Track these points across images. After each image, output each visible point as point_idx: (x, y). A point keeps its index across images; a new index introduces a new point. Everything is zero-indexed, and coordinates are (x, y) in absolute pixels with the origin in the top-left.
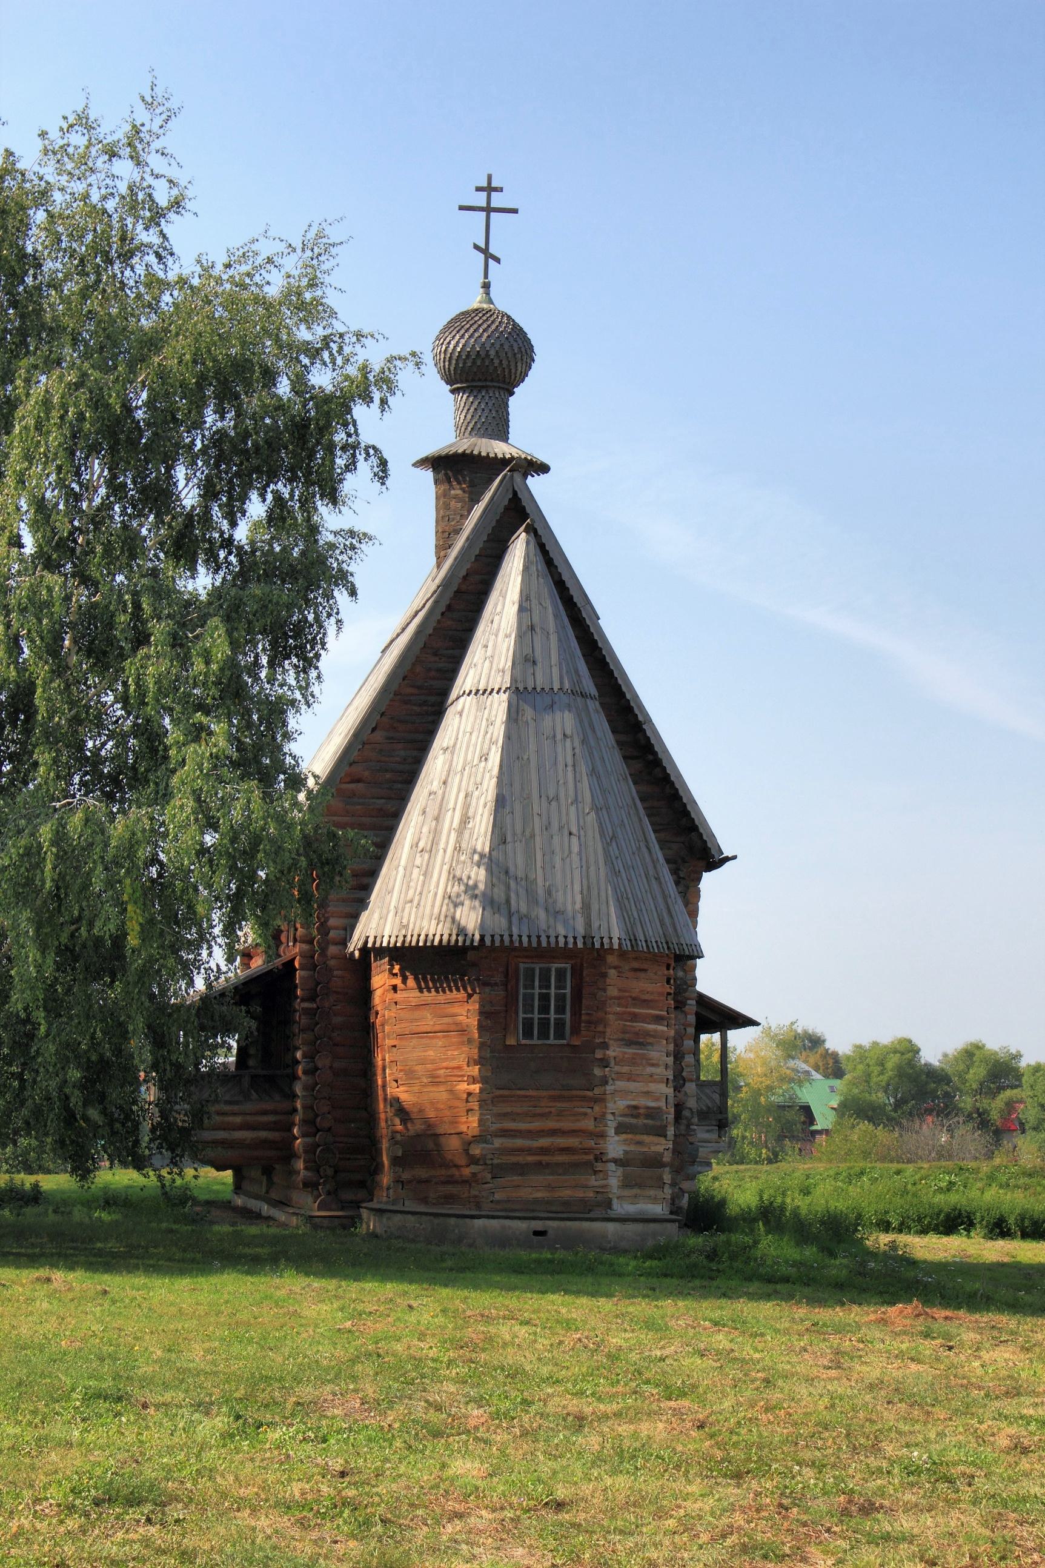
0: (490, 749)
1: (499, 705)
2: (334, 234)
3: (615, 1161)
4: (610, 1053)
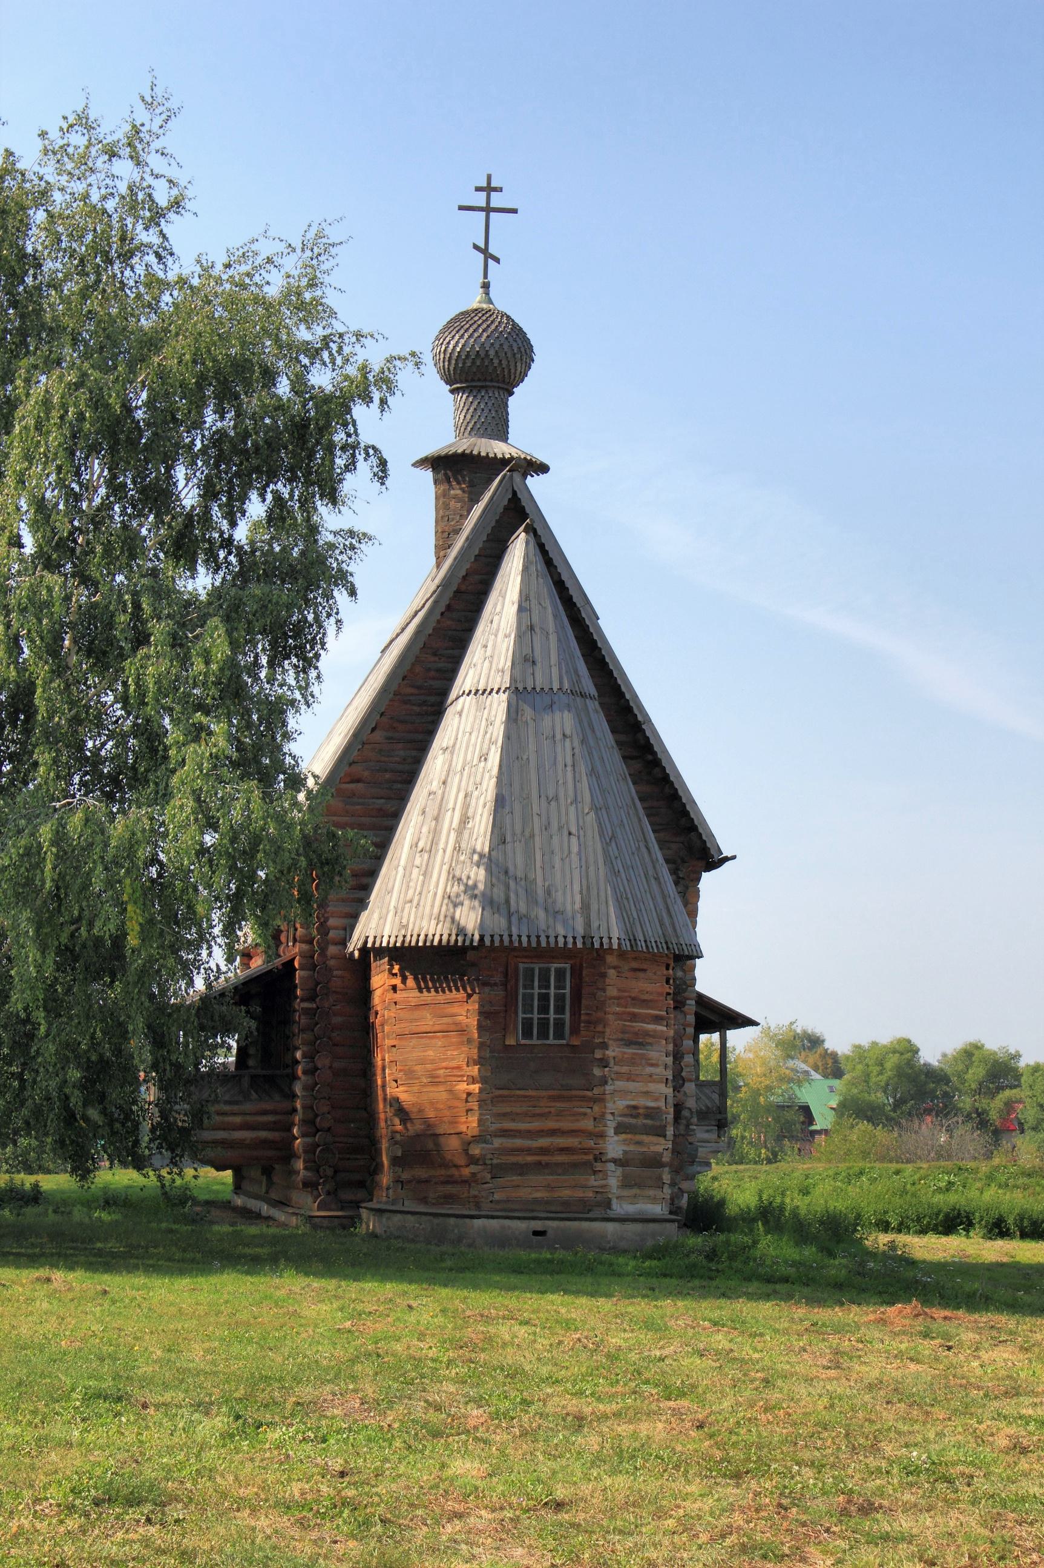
0: (489, 749)
1: (499, 705)
2: (334, 234)
3: (614, 1161)
4: (610, 1053)
